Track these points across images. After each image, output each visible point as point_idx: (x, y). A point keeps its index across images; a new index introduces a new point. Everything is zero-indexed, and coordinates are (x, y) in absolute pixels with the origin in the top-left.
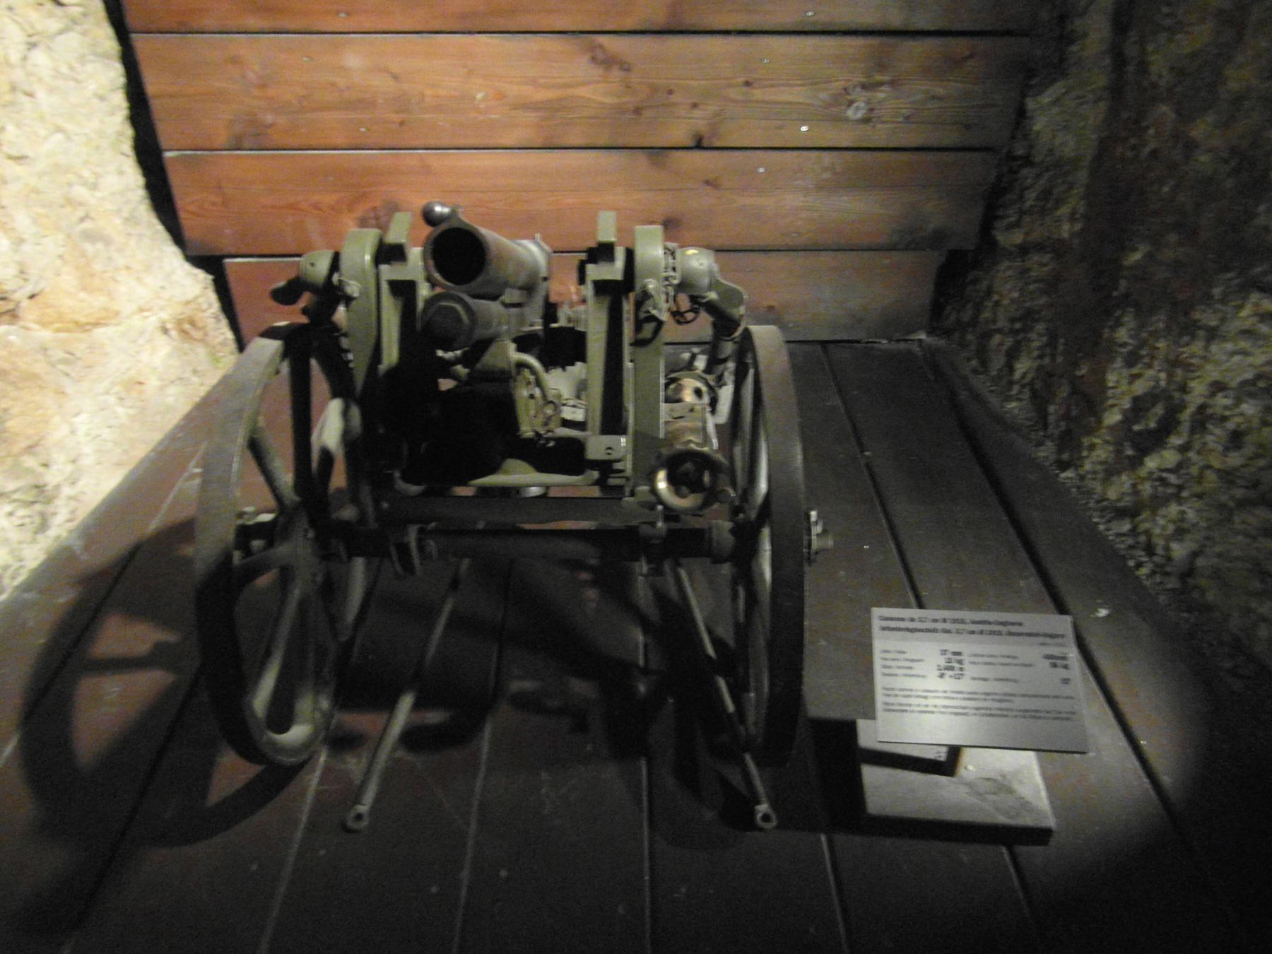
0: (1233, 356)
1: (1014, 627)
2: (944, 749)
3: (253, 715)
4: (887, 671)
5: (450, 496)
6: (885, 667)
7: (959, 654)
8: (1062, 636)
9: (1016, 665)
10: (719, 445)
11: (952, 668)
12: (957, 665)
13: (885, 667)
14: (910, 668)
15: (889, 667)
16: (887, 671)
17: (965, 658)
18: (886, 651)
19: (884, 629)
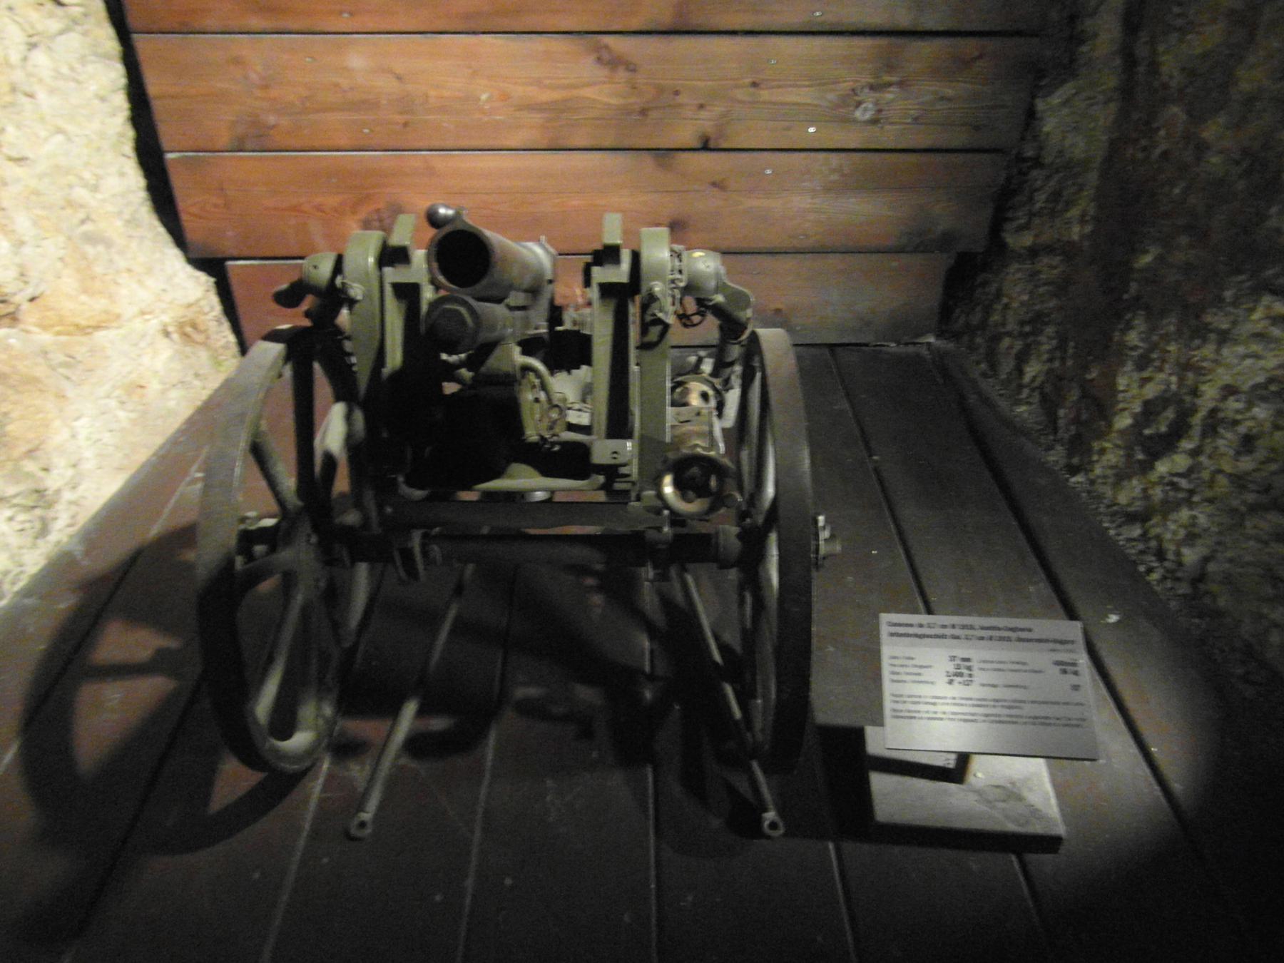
0: (1244, 360)
1: (1023, 633)
2: (953, 757)
3: (256, 721)
4: (895, 677)
5: (454, 501)
6: (893, 673)
7: (968, 660)
8: (1072, 642)
9: (1025, 671)
10: (726, 449)
11: (961, 675)
12: (966, 672)
13: (893, 673)
14: (919, 674)
15: (898, 673)
16: (895, 677)
17: (974, 664)
18: (894, 658)
19: (892, 635)
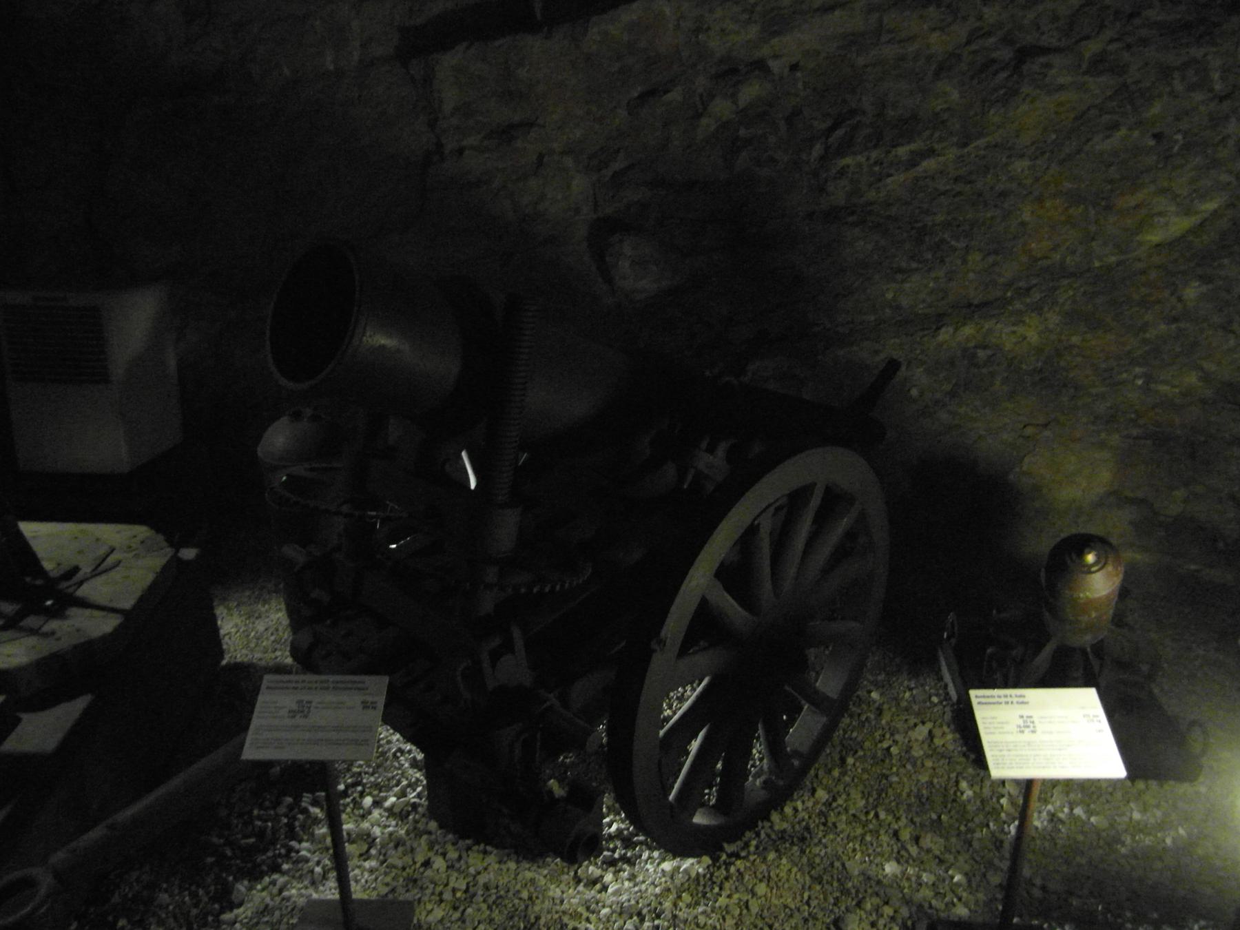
14: (1002, 728)
